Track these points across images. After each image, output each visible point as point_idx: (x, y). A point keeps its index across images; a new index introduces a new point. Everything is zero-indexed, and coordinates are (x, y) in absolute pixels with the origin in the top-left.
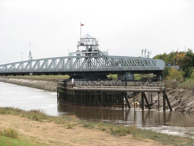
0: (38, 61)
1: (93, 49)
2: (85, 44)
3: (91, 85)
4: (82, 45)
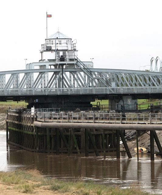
1: (67, 57)
2: (53, 48)
4: (49, 49)
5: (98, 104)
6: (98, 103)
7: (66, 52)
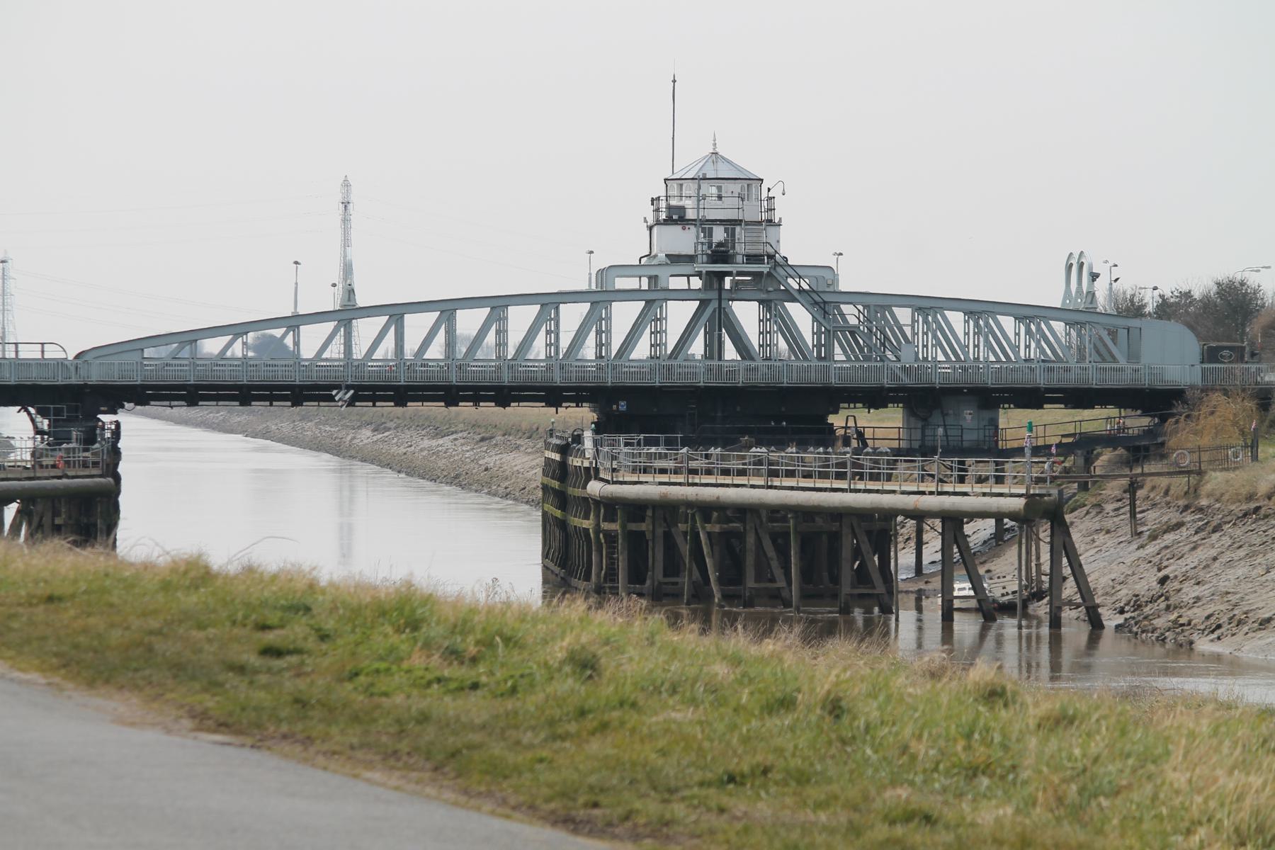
0: (396, 314)
1: (740, 248)
2: (691, 214)
3: (85, 465)
4: (676, 217)
5: (851, 424)
6: (851, 419)
7: (738, 229)
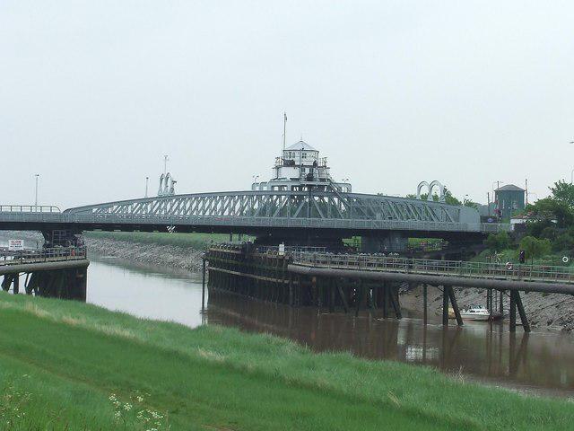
4: (291, 164)
